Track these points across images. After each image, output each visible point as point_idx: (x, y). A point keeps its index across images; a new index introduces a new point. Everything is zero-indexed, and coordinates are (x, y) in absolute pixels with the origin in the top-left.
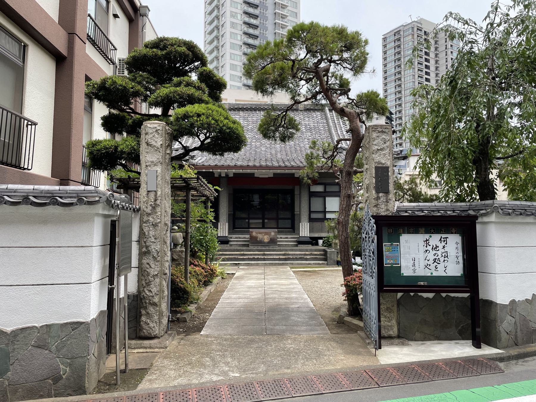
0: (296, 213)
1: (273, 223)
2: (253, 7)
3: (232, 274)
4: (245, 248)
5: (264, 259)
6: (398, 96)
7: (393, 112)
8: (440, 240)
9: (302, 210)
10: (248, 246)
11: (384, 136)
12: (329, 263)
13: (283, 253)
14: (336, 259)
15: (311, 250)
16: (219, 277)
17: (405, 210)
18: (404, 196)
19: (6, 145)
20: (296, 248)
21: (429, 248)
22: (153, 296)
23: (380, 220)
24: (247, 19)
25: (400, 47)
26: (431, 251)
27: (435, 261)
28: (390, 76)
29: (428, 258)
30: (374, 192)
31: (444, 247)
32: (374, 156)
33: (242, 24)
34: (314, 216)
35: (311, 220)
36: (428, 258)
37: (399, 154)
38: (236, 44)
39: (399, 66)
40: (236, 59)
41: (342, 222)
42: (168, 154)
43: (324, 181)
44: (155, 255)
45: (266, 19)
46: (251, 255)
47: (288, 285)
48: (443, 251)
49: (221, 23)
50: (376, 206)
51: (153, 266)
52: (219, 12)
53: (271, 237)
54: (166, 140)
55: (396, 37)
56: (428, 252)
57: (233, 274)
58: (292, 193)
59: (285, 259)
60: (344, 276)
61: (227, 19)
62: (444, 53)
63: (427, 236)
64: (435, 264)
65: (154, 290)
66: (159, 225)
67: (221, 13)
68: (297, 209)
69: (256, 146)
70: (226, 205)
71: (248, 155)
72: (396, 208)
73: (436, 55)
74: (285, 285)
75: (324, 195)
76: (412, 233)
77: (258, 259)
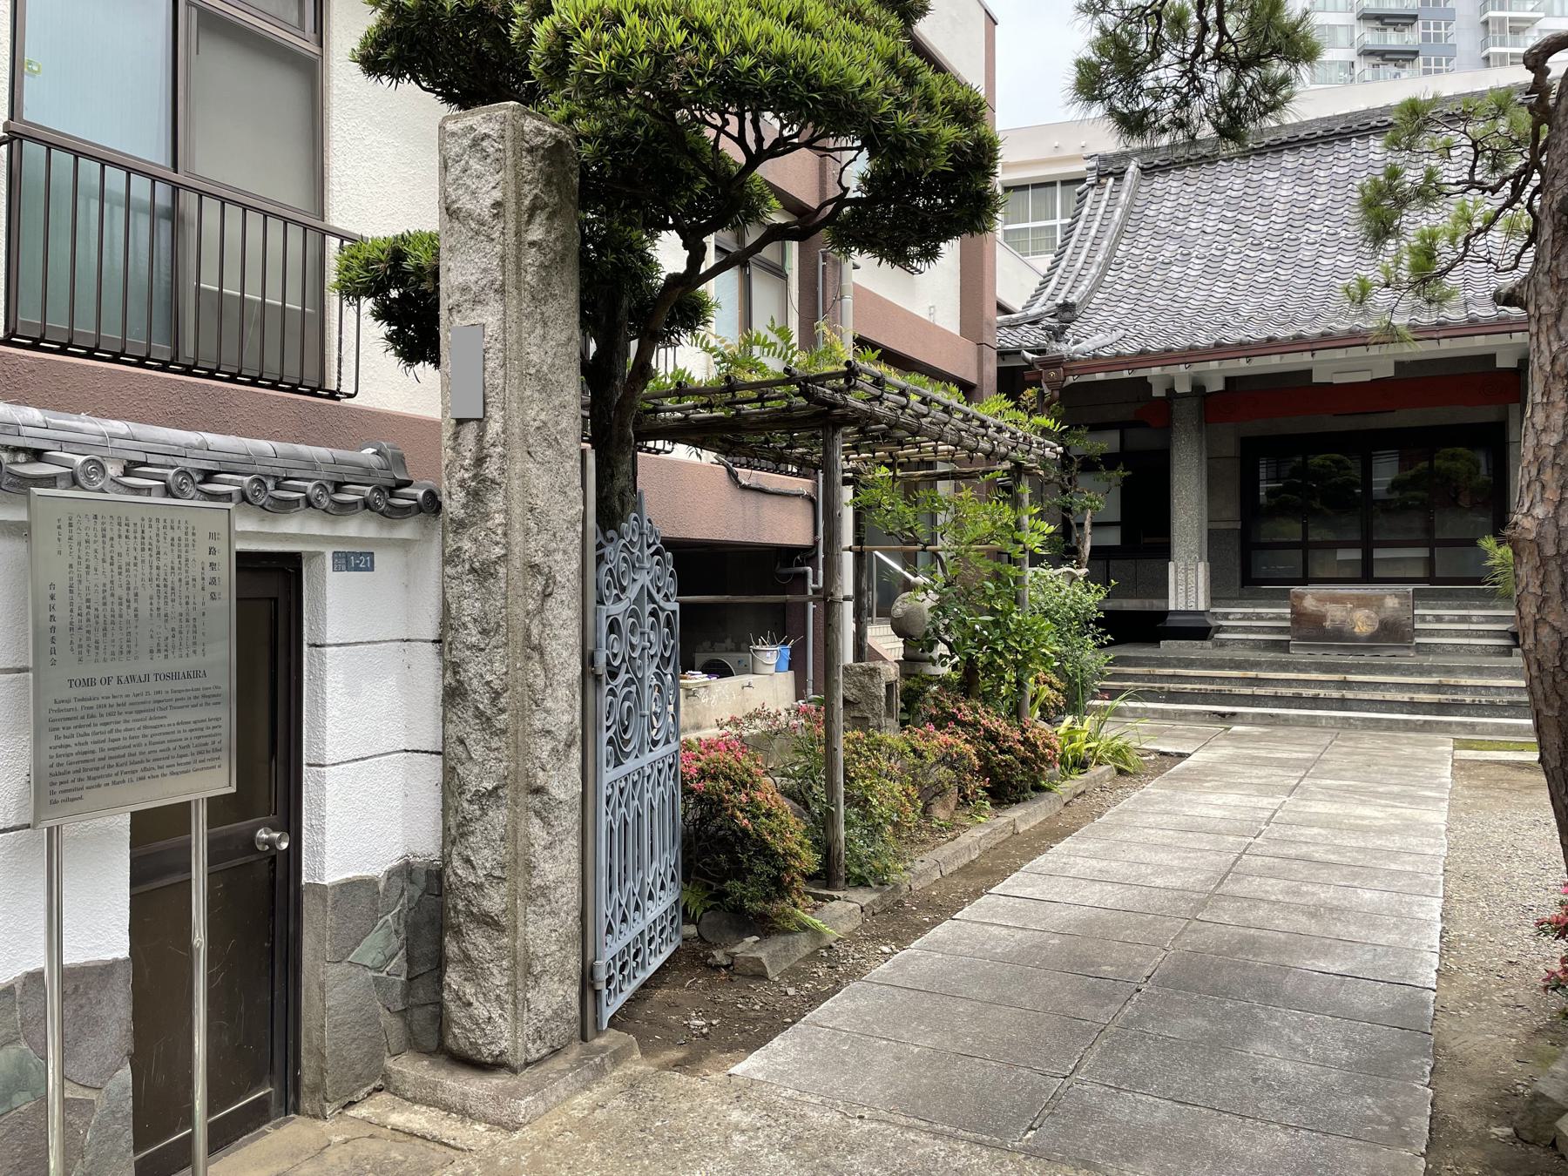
4: (1270, 656)
5: (1343, 704)
10: (1282, 646)
19: (293, 326)
22: (479, 887)
41: (1538, 544)
42: (532, 244)
44: (484, 703)
47: (1382, 831)
51: (478, 752)
54: (519, 179)
59: (1441, 708)
65: (486, 858)
66: (502, 571)
70: (1194, 499)
74: (1364, 830)
77: (1315, 702)
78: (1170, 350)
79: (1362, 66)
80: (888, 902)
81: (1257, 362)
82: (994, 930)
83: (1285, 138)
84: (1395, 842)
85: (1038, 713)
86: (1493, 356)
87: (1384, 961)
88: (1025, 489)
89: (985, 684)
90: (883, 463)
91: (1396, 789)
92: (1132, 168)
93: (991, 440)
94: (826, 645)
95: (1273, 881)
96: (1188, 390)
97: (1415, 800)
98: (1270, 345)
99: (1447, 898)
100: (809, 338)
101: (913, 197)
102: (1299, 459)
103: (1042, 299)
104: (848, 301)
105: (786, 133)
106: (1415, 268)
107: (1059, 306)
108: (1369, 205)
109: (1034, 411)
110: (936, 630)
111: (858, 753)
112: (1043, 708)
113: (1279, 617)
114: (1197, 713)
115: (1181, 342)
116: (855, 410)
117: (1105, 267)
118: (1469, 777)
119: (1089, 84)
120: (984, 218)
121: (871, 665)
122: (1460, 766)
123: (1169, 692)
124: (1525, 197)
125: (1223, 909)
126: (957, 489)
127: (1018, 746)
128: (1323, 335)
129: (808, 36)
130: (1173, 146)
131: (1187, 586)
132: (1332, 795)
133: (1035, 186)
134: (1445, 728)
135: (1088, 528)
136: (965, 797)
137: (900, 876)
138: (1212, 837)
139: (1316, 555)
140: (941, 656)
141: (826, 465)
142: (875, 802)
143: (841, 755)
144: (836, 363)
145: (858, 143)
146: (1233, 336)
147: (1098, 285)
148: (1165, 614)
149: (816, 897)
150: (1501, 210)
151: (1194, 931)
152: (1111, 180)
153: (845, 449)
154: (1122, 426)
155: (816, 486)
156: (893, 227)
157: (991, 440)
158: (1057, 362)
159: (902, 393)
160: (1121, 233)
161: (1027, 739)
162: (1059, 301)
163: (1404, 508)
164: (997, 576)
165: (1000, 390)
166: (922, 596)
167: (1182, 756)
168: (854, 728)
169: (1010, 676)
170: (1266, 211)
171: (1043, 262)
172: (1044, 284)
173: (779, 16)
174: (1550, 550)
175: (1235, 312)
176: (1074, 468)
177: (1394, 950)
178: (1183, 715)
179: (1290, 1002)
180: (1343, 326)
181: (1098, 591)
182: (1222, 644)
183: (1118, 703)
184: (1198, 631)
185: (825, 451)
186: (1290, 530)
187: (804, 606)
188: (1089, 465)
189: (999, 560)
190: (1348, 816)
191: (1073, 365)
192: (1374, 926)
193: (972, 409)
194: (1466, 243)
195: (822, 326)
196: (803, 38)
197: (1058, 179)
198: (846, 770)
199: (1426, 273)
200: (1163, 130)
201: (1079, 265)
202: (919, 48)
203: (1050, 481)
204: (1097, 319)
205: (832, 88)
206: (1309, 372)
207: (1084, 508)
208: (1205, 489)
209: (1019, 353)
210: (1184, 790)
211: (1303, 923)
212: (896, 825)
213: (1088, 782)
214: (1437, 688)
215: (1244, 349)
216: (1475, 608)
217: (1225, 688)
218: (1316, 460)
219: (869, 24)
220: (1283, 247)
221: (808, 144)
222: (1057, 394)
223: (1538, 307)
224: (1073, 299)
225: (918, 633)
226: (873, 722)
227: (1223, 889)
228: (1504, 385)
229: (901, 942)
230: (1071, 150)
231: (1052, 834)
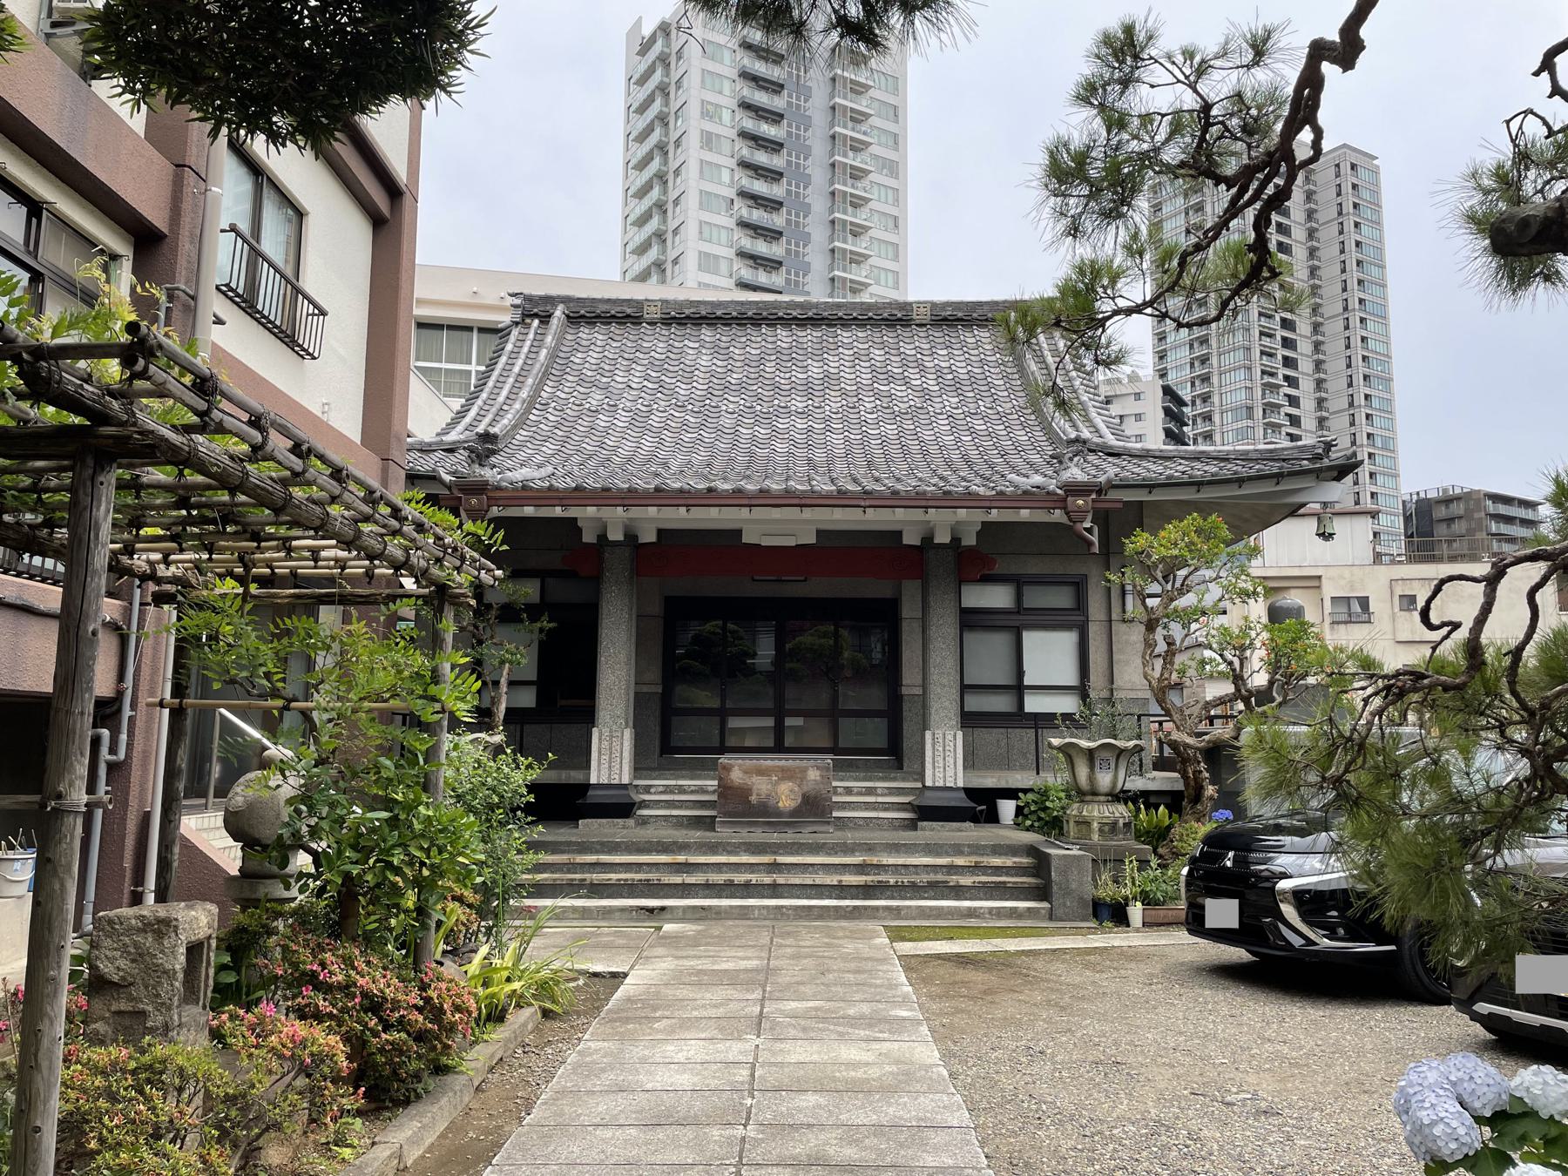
0: (905, 691)
1: (819, 733)
2: (766, 89)
3: (614, 975)
4: (697, 835)
5: (775, 890)
7: (1187, 399)
9: (934, 676)
12: (1059, 912)
14: (1089, 891)
15: (976, 849)
16: (527, 1012)
20: (908, 837)
24: (749, 124)
33: (735, 137)
34: (976, 703)
35: (970, 720)
37: (1318, 457)
38: (717, 196)
40: (715, 238)
43: (1014, 568)
45: (807, 123)
46: (718, 867)
49: (674, 136)
52: (667, 104)
57: (618, 977)
59: (867, 891)
61: (692, 125)
62: (1335, 229)
67: (674, 106)
70: (622, 657)
71: (718, 464)
73: (1311, 234)
75: (1014, 623)
77: (748, 890)
78: (607, 490)
81: (697, 513)
83: (704, 313)
86: (900, 533)
91: (865, 1009)
96: (621, 538)
103: (460, 427)
110: (296, 834)
112: (450, 937)
114: (623, 910)
117: (530, 404)
123: (592, 884)
126: (346, 619)
131: (611, 757)
133: (450, 327)
134: (872, 913)
135: (504, 688)
140: (301, 875)
147: (521, 422)
152: (536, 322)
160: (546, 374)
161: (428, 1000)
162: (480, 429)
164: (405, 754)
169: (410, 900)
171: (457, 404)
175: (665, 465)
178: (607, 913)
181: (529, 766)
182: (644, 822)
184: (620, 807)
186: (705, 697)
191: (498, 494)
197: (475, 325)
201: (501, 399)
204: (521, 456)
206: (739, 532)
207: (502, 663)
208: (633, 648)
214: (861, 868)
215: (685, 498)
216: (857, 779)
217: (653, 876)
220: (706, 414)
224: (495, 430)
225: (267, 834)
226: (155, 1020)
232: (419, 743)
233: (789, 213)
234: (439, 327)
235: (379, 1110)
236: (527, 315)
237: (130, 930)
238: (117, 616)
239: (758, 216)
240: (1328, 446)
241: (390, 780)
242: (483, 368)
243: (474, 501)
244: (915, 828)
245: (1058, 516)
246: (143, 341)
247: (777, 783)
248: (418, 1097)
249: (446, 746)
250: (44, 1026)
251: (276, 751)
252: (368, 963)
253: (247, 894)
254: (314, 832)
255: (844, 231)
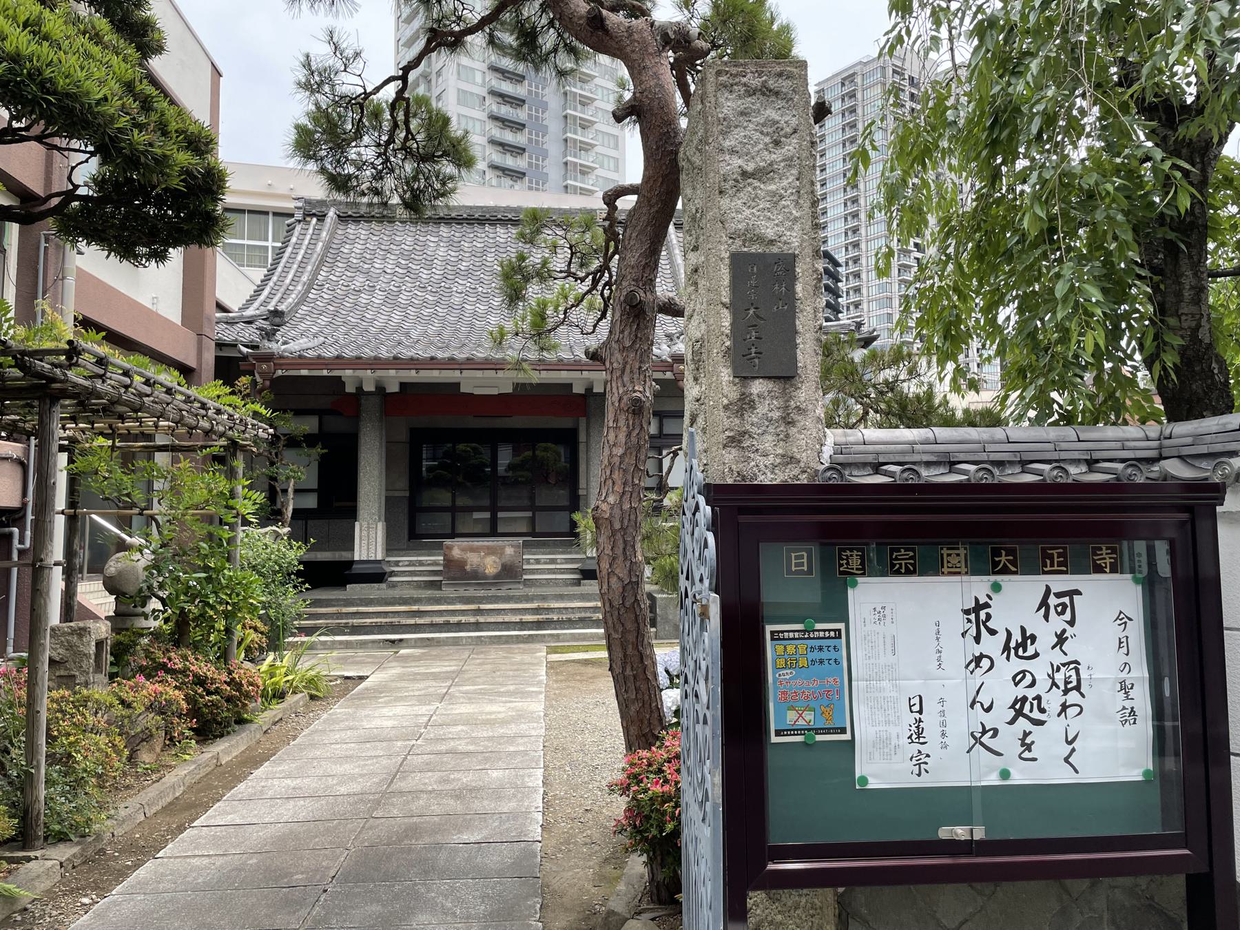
4: (428, 593)
5: (477, 626)
6: (852, 223)
7: (841, 260)
8: (1044, 603)
11: (772, 114)
12: (661, 634)
13: (534, 605)
17: (870, 459)
18: (867, 413)
21: (992, 646)
23: (744, 512)
25: (855, 111)
26: (1000, 659)
27: (1019, 713)
28: (834, 177)
29: (984, 698)
30: (726, 374)
31: (1061, 639)
32: (725, 202)
36: (984, 698)
38: (472, 94)
39: (855, 215)
46: (440, 613)
47: (504, 722)
48: (1058, 658)
50: (735, 441)
53: (506, 559)
55: (846, 90)
56: (985, 663)
58: (569, 440)
59: (539, 625)
60: (630, 746)
63: (979, 586)
64: (1022, 723)
68: (582, 483)
69: (475, 313)
70: (376, 473)
71: (446, 334)
72: (828, 451)
76: (909, 573)
77: (459, 627)
79: (490, 174)
80: (90, 852)
81: (423, 373)
82: (194, 861)
84: (512, 729)
85: (243, 655)
87: (507, 825)
88: (239, 464)
89: (196, 634)
90: (101, 434)
91: (512, 688)
92: (331, 213)
93: (210, 420)
94: (33, 610)
95: (430, 774)
96: (373, 389)
97: (524, 695)
98: (432, 362)
99: (546, 767)
100: (27, 313)
101: (144, 204)
102: (450, 445)
103: (256, 304)
104: (71, 282)
105: (15, 125)
106: (534, 325)
107: (271, 312)
108: (506, 276)
109: (248, 395)
110: (150, 588)
111: (61, 711)
112: (248, 650)
113: (435, 563)
114: (373, 642)
115: (368, 353)
116: (76, 385)
117: (310, 286)
118: (557, 674)
119: (305, 144)
120: (212, 235)
121: (81, 624)
122: (551, 666)
124: (600, 288)
125: (393, 805)
126: (175, 461)
127: (225, 687)
128: (468, 359)
129: (45, 44)
130: (370, 205)
131: (369, 541)
132: (470, 698)
133: (250, 212)
136: (171, 739)
137: (103, 825)
138: (384, 744)
139: (459, 515)
140: (154, 611)
141: (42, 434)
142: (79, 757)
143: (44, 716)
144: (56, 339)
145: (90, 148)
146: (407, 353)
147: (303, 300)
148: (352, 562)
149: (11, 860)
150: (586, 294)
151: (371, 828)
152: (315, 220)
153: (62, 419)
154: (320, 413)
155: (27, 452)
156: (123, 227)
157: (210, 420)
158: (268, 358)
159: (126, 373)
160: (322, 262)
161: (233, 679)
163: (515, 483)
165: (217, 377)
166: (137, 556)
167: (362, 678)
168: (59, 687)
169: (221, 625)
170: (430, 265)
171: (258, 274)
172: (258, 292)
173: (15, 18)
174: (617, 526)
175: (407, 335)
176: (281, 444)
177: (514, 815)
178: (363, 644)
179: (443, 874)
180: (480, 354)
181: (299, 547)
182: (394, 586)
183: (314, 638)
184: (376, 576)
185: (41, 422)
186: (443, 497)
187: (8, 572)
188: (293, 442)
189: (211, 523)
190: (481, 713)
191: (282, 361)
192: (499, 798)
193: (193, 392)
194: (565, 313)
195: (42, 304)
196: (41, 44)
197: (270, 210)
198: (48, 729)
199: (540, 330)
200: (363, 194)
201: (288, 281)
202: (153, 81)
203: (260, 454)
204: (302, 326)
205: (68, 95)
206: (458, 384)
207: (288, 478)
209: (236, 346)
210: (364, 707)
211: (453, 805)
212: (99, 776)
213: (285, 710)
214: (537, 611)
215: (414, 363)
218: (461, 447)
219: (106, 47)
220: (442, 293)
221: (39, 139)
222: (268, 383)
223: (611, 363)
224: (282, 307)
225: (131, 589)
227: (394, 787)
228: (588, 404)
229: (102, 890)
230: (282, 190)
231: (252, 761)
232: (225, 533)
233: (530, 109)
234: (242, 211)
235: (206, 740)
236: (308, 215)
237: (64, 634)
238: (20, 454)
239: (505, 111)
240: (859, 325)
241: (206, 555)
242: (279, 245)
243: (264, 366)
244: (579, 584)
245: (669, 375)
246: (75, 348)
247: (484, 557)
248: (229, 733)
249: (241, 535)
250: (39, 665)
251: (137, 541)
252: (197, 659)
253: (120, 626)
254: (162, 586)
255: (575, 124)
